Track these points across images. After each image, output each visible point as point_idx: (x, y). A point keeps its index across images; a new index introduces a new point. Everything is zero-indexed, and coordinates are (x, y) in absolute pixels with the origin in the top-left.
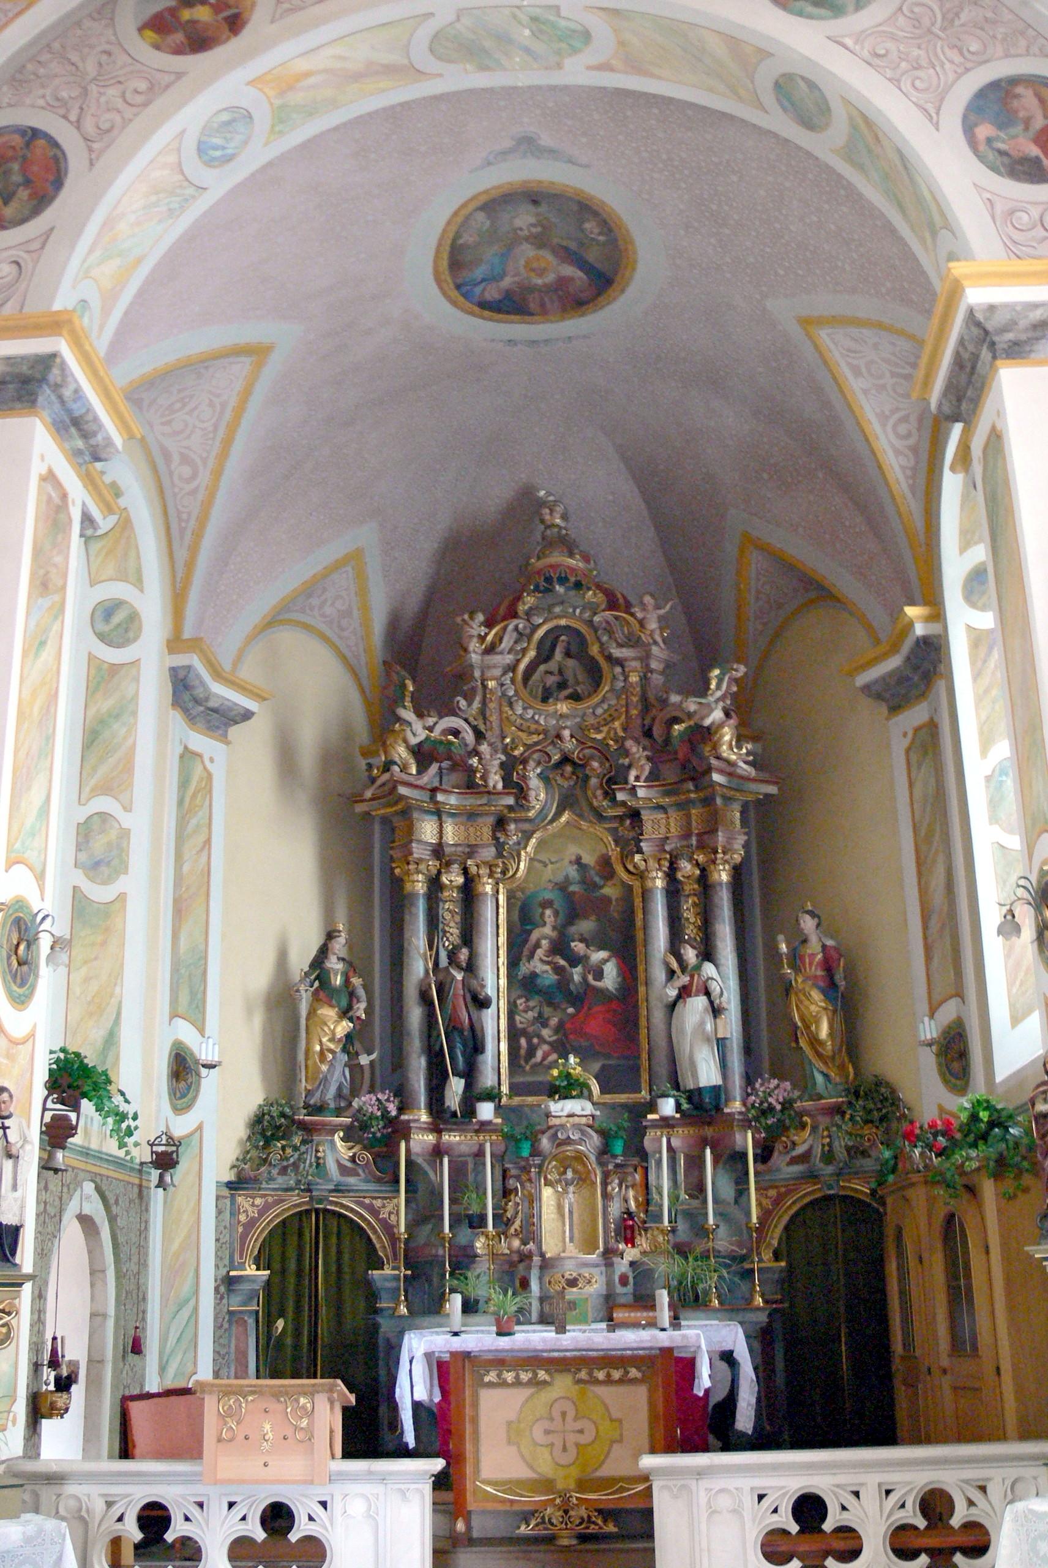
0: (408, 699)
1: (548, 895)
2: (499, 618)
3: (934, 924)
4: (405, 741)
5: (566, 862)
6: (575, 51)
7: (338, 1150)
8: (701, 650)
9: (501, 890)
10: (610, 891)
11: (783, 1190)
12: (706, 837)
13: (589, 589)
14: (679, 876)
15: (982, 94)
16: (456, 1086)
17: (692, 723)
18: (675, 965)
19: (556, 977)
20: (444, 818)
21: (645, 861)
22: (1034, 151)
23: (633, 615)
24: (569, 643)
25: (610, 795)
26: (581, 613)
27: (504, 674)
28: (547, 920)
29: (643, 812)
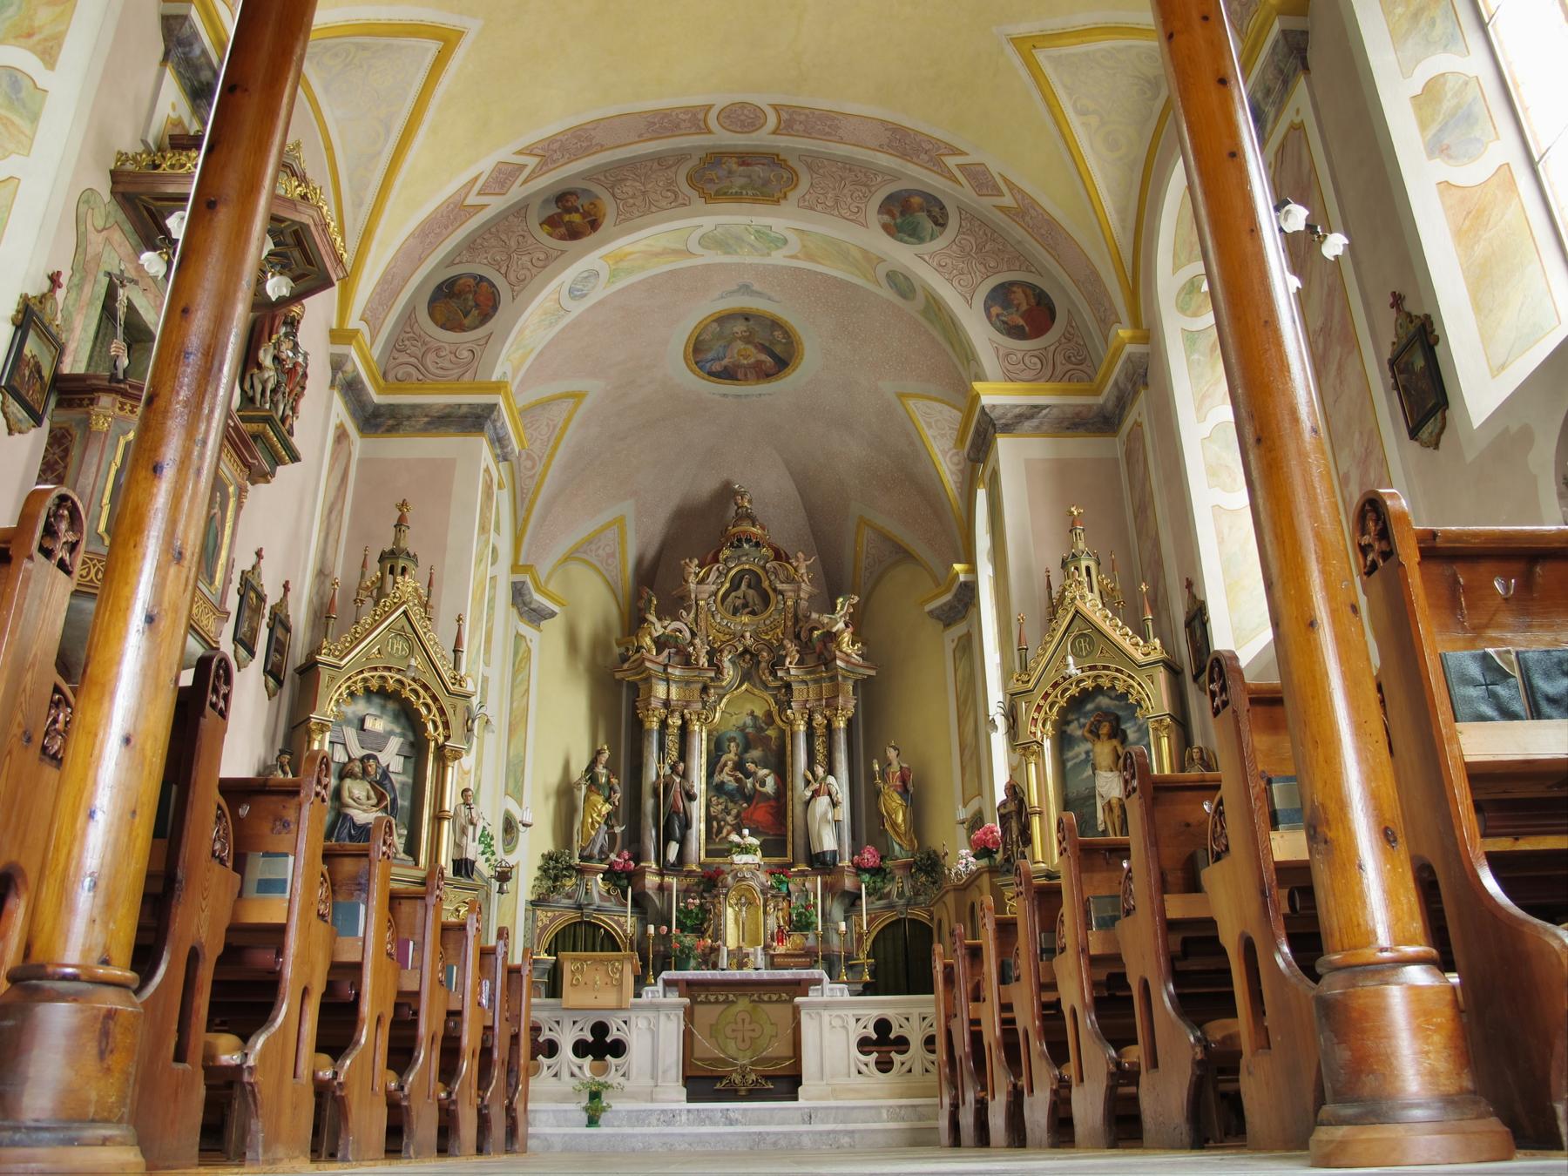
3: (967, 753)
6: (778, 248)
7: (598, 884)
8: (831, 588)
10: (771, 732)
15: (995, 290)
16: (673, 850)
22: (1021, 322)
25: (773, 673)
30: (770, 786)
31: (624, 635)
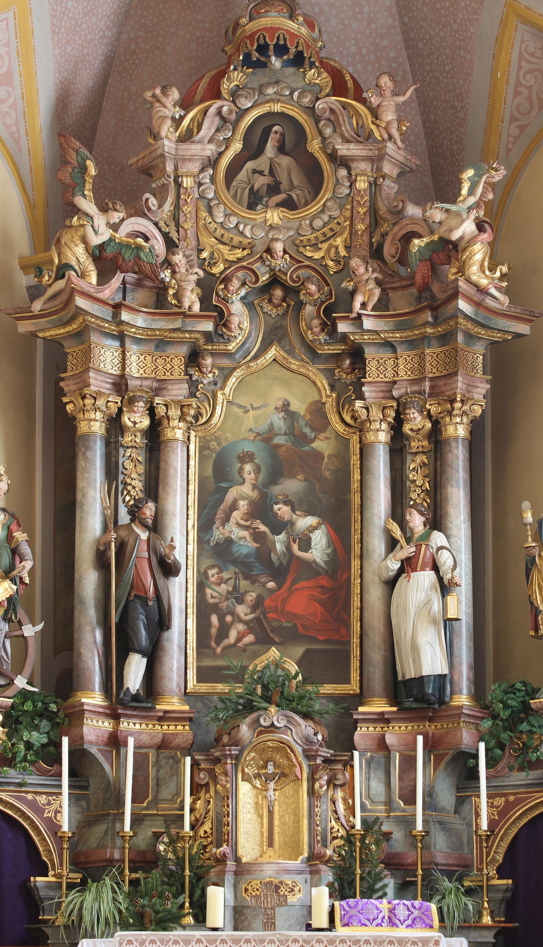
0: (88, 186)
1: (248, 447)
2: (198, 97)
4: (84, 240)
5: (272, 407)
9: (192, 438)
10: (323, 445)
11: (512, 798)
12: (441, 383)
13: (312, 65)
14: (406, 428)
16: (135, 669)
17: (436, 237)
18: (397, 533)
19: (255, 545)
20: (128, 344)
21: (367, 409)
23: (364, 101)
24: (283, 135)
26: (299, 97)
27: (202, 170)
28: (246, 476)
29: (366, 350)
30: (319, 548)
31: (35, 250)
